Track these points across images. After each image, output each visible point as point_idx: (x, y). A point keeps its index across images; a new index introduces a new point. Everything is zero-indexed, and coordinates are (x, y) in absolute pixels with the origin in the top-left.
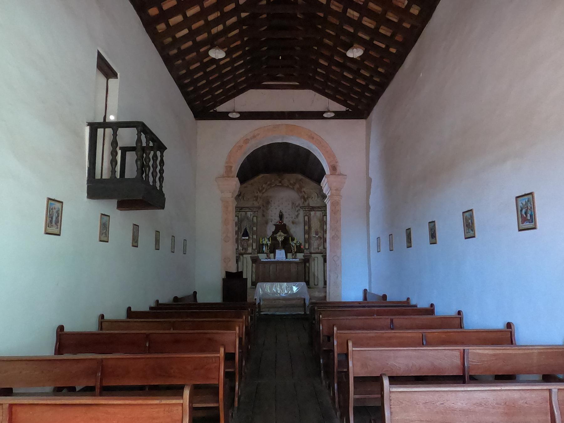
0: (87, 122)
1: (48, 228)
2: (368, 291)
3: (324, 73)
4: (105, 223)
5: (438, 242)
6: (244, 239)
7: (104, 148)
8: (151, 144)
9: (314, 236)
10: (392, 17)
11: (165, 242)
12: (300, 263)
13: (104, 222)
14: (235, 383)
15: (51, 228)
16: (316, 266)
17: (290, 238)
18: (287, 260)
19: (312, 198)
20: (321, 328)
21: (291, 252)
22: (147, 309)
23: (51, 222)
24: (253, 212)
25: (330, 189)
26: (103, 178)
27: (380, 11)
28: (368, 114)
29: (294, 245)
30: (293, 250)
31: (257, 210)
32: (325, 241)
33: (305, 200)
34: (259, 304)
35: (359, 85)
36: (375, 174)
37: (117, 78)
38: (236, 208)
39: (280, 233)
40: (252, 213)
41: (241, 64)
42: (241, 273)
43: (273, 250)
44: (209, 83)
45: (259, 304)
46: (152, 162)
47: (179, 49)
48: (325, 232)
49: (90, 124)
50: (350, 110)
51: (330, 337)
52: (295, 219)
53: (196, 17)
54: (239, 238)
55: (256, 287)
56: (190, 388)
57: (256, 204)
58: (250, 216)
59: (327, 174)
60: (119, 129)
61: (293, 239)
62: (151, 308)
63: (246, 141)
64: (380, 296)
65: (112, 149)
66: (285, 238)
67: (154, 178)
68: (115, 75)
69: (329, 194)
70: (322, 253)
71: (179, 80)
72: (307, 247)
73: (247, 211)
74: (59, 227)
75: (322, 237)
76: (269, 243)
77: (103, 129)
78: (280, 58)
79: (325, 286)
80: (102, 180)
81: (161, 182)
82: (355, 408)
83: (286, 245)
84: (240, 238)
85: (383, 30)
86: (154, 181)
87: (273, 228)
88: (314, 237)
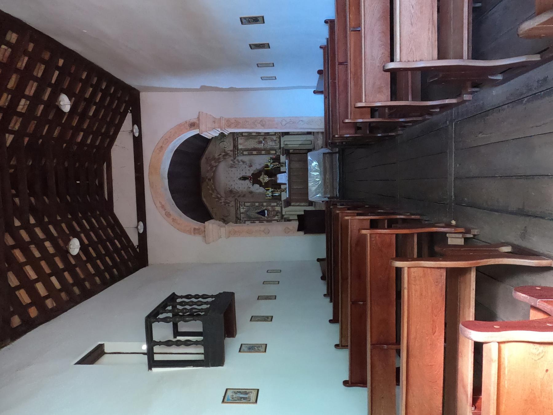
0: (148, 371)
1: (251, 401)
2: (315, 89)
3: (91, 136)
4: (248, 348)
5: (262, 15)
6: (267, 214)
7: (180, 352)
8: (170, 308)
9: (263, 145)
10: (22, 64)
11: (270, 290)
12: (289, 158)
13: (248, 349)
14: (398, 218)
15: (252, 399)
16: (292, 143)
17: (265, 169)
18: (287, 172)
19: (224, 147)
20: (348, 136)
21: (279, 168)
22: (332, 304)
23: (244, 398)
24: (240, 206)
25: (214, 129)
26: (203, 352)
27: (16, 77)
28: (134, 89)
29: (272, 165)
30: (277, 166)
31: (238, 202)
32: (267, 134)
33: (227, 154)
34: (329, 198)
35: (103, 99)
36: (196, 82)
37: (104, 344)
38: (237, 223)
39: (261, 179)
40: (242, 207)
41: (87, 222)
42: (299, 216)
43: (277, 186)
44: (108, 253)
45: (329, 198)
46: (187, 306)
47: (73, 285)
48: (259, 134)
49: (150, 368)
50: (131, 109)
51: (357, 127)
52: (247, 165)
53: (38, 269)
54: (266, 219)
55: (314, 202)
56: (394, 261)
57: (233, 203)
58: (245, 209)
59: (198, 133)
60: (154, 340)
61: (267, 166)
62: (331, 301)
63: (168, 215)
64: (320, 76)
65: (183, 346)
66: (265, 174)
67: (203, 303)
68: (101, 347)
69: (219, 130)
70: (280, 136)
71: (106, 284)
72: (273, 152)
73: (240, 212)
74: (250, 391)
75: (263, 137)
76: (271, 190)
77: (155, 355)
78: (77, 182)
79: (312, 133)
80: (206, 354)
81: (208, 297)
82: (423, 100)
83: (273, 173)
84: (266, 218)
85: (39, 71)
86: (206, 303)
87: (257, 186)
88: (264, 145)
